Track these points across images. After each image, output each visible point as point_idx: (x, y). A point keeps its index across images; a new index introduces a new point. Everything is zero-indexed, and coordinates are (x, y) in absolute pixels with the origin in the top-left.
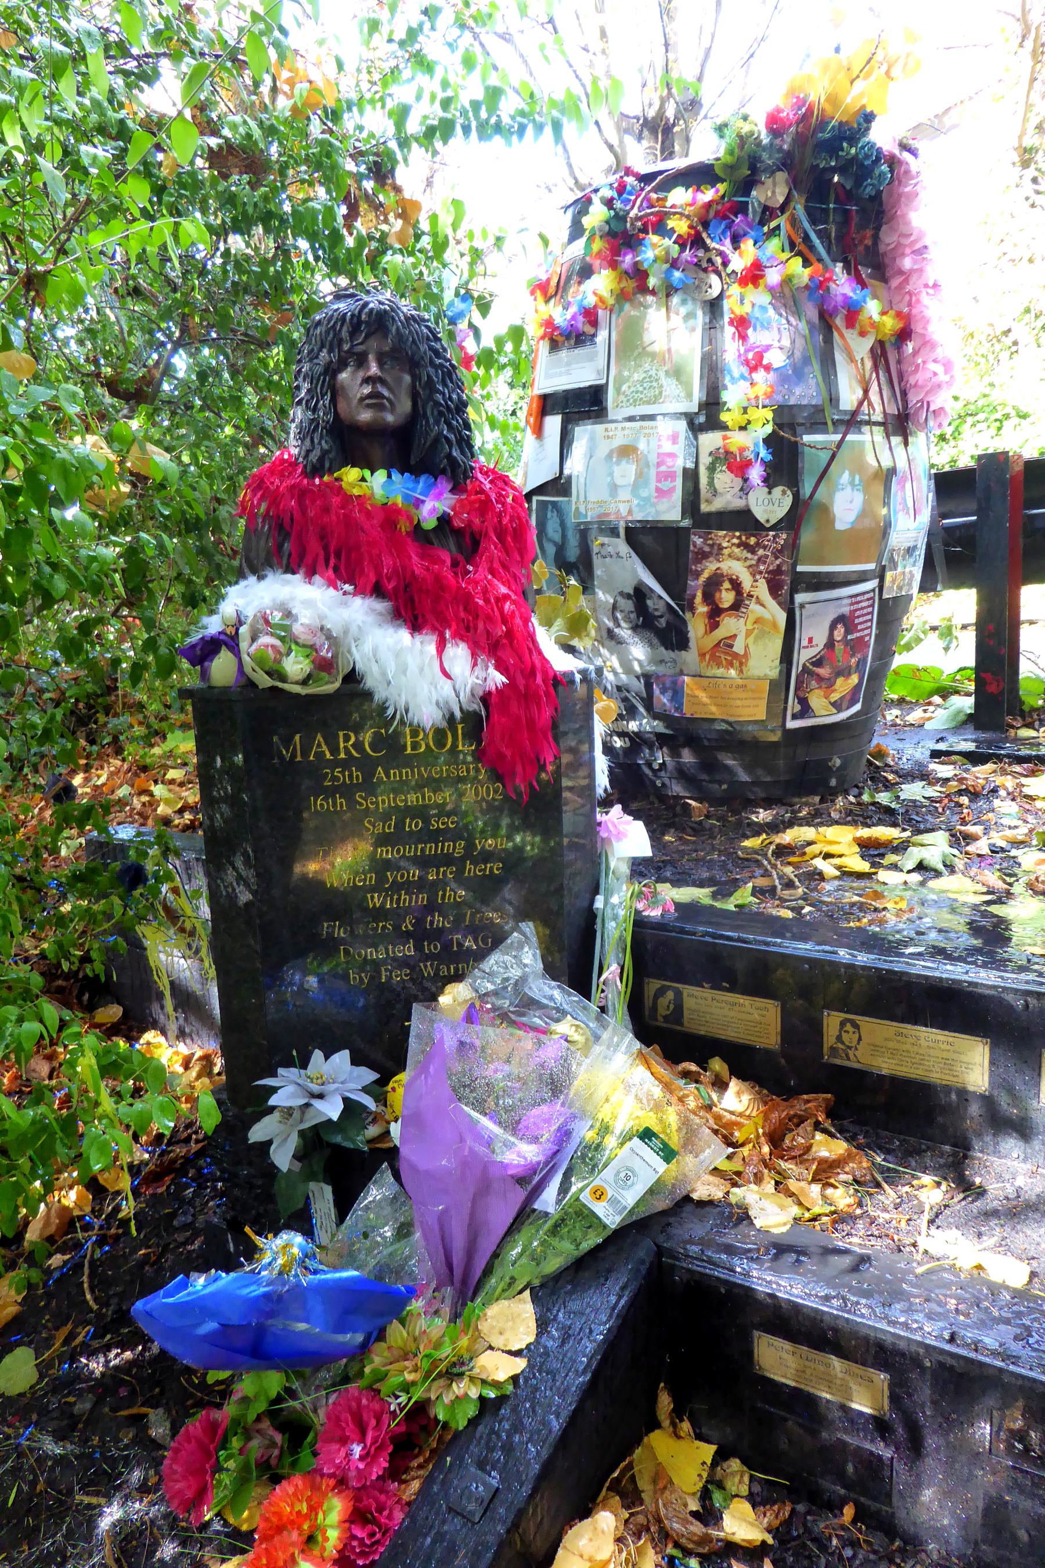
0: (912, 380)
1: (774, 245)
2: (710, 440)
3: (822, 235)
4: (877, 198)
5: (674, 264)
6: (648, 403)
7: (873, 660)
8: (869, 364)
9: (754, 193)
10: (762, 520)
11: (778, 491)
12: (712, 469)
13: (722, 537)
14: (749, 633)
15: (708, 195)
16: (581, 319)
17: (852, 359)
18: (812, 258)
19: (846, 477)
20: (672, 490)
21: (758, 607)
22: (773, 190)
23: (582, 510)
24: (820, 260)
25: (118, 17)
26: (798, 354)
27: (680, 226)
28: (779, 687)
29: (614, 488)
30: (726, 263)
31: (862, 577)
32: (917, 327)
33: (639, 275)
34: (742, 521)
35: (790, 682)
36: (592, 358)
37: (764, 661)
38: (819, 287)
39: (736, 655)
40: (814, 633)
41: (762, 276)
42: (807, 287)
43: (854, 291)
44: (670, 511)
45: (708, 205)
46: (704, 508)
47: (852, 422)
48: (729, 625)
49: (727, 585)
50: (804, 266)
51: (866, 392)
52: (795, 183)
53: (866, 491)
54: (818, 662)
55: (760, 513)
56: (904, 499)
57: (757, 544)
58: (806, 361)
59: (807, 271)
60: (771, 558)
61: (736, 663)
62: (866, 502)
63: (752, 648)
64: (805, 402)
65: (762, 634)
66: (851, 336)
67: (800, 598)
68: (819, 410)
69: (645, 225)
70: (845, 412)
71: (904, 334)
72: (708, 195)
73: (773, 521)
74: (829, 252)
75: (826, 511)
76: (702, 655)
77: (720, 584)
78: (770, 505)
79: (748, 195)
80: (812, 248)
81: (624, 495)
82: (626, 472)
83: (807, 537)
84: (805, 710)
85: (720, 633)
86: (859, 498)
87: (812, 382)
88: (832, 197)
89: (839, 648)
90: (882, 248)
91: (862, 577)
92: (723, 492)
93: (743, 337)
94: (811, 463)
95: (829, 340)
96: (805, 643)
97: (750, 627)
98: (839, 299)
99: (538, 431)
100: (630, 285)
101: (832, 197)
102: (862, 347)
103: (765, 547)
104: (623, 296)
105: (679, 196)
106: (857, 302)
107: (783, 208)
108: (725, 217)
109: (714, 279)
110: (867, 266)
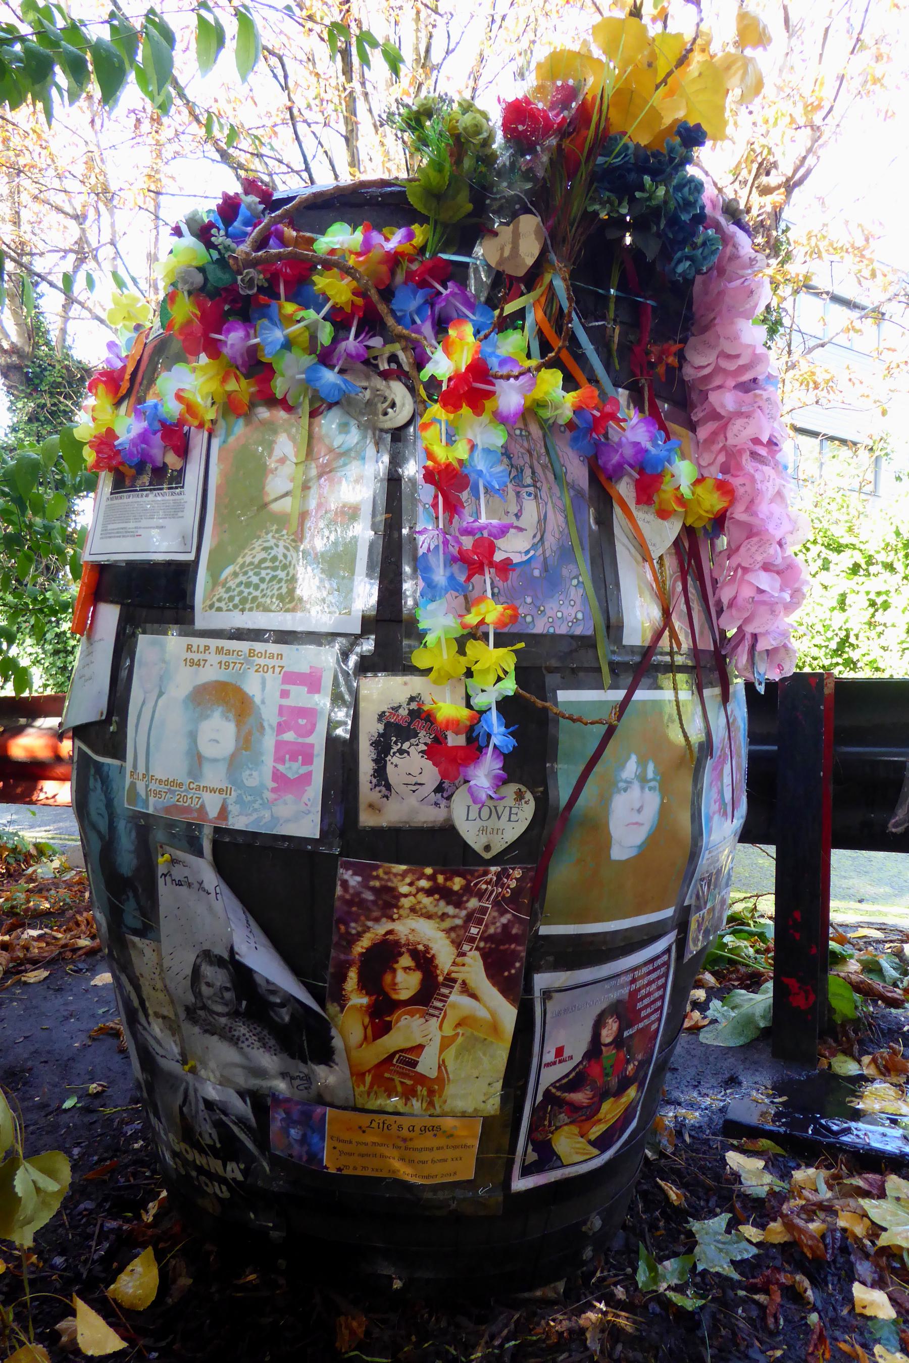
0: (726, 595)
1: (512, 344)
2: (384, 692)
3: (600, 338)
4: (682, 290)
5: (326, 358)
7: (659, 1053)
8: (671, 564)
9: (479, 250)
10: (478, 847)
12: (382, 747)
13: (401, 877)
14: (446, 1043)
15: (394, 241)
16: (157, 439)
17: (646, 557)
18: (581, 377)
19: (631, 768)
20: (306, 778)
21: (465, 1000)
22: (520, 240)
23: (141, 787)
24: (593, 380)
25: (368, 394)
26: (551, 541)
27: (336, 289)
28: (499, 1131)
29: (197, 760)
30: (421, 362)
31: (651, 934)
32: (739, 513)
33: (256, 368)
34: (438, 849)
35: (523, 1111)
36: (176, 511)
37: (475, 1088)
38: (590, 429)
39: (422, 1079)
40: (566, 1040)
41: (490, 394)
42: (571, 425)
43: (653, 439)
44: (300, 817)
45: (394, 260)
46: (366, 819)
47: (644, 667)
48: (409, 1029)
49: (406, 961)
50: (566, 388)
51: (667, 614)
52: (553, 239)
53: (664, 789)
54: (575, 1082)
55: (472, 833)
56: (721, 793)
57: (468, 890)
58: (566, 554)
59: (570, 398)
60: (491, 913)
61: (422, 1091)
62: (663, 811)
63: (451, 1065)
64: (562, 630)
65: (473, 1044)
66: (645, 518)
67: (542, 980)
68: (587, 643)
69: (273, 279)
70: (632, 649)
71: (719, 522)
72: (394, 241)
73: (494, 851)
74: (608, 366)
75: (597, 830)
76: (358, 1075)
78: (489, 815)
79: (469, 254)
80: (581, 359)
81: (214, 776)
82: (219, 733)
83: (563, 873)
84: (547, 1157)
85: (393, 1041)
86: (652, 801)
87: (575, 594)
89: (609, 1053)
90: (689, 373)
91: (651, 934)
92: (408, 792)
93: (453, 508)
94: (574, 745)
95: (605, 522)
96: (549, 1057)
97: (448, 1031)
98: (628, 452)
99: (85, 627)
100: (241, 387)
101: (615, 278)
102: (662, 535)
103: (480, 895)
104: (231, 407)
105: (340, 237)
106: (659, 461)
107: (532, 278)
108: (423, 284)
109: (398, 390)
110: (666, 400)
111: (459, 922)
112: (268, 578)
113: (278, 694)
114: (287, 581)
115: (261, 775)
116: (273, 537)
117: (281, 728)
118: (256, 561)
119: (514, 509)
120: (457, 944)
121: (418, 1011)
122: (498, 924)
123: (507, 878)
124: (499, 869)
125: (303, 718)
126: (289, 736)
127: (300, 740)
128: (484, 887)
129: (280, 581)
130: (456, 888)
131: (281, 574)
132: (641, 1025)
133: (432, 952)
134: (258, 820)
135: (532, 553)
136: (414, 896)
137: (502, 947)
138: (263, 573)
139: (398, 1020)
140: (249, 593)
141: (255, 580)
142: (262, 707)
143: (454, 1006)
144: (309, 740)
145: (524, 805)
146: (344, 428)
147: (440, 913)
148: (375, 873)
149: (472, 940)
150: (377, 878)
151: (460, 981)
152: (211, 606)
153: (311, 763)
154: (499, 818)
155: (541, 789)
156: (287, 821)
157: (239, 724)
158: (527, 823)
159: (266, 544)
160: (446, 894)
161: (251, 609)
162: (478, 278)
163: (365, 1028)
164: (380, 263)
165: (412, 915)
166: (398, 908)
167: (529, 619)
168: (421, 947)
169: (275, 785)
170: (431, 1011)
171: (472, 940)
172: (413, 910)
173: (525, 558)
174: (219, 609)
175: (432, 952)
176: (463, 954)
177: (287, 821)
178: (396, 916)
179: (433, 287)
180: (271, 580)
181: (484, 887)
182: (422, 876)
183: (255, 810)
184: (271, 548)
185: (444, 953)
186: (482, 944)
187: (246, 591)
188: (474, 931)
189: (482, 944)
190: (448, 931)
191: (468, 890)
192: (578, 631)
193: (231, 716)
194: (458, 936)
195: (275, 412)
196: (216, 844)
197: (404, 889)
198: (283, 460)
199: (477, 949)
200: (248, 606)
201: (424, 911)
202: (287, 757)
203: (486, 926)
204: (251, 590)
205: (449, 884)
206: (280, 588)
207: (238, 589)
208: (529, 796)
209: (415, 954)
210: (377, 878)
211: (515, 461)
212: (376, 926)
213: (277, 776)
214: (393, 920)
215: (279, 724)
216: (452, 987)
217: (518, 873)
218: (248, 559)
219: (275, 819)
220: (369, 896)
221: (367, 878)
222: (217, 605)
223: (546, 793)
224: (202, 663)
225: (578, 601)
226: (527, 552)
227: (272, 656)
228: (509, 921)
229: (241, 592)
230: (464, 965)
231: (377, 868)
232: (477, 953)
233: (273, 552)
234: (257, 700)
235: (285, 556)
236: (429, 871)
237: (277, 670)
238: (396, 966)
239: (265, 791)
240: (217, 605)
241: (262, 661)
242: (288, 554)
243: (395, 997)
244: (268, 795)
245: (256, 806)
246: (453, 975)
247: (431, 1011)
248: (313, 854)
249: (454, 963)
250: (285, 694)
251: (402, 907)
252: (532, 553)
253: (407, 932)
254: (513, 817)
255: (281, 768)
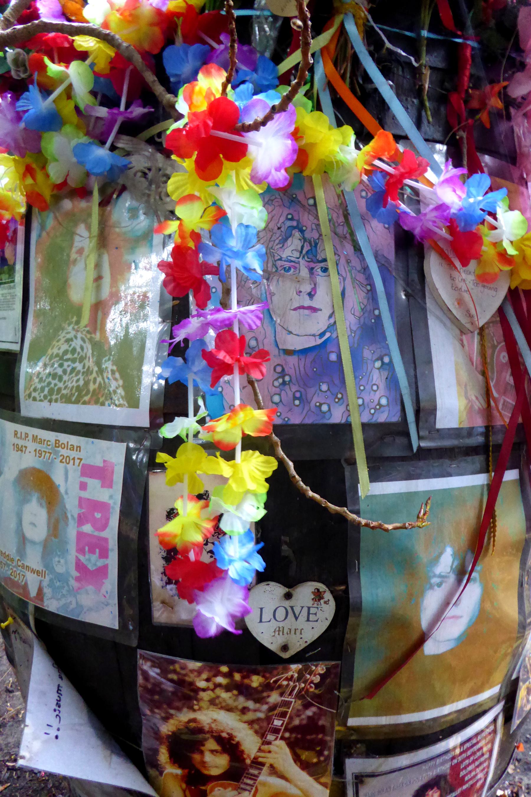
6: (67, 400)
11: (305, 592)
20: (103, 571)
49: (211, 744)
55: (266, 634)
67: (354, 765)
74: (418, 124)
77: (202, 743)
80: (380, 109)
81: (33, 559)
88: (426, 17)
101: (426, 17)
111: (261, 715)
112: (69, 370)
113: (78, 486)
114: (83, 373)
115: (66, 564)
116: (73, 328)
117: (81, 520)
118: (61, 352)
119: (307, 288)
120: (262, 734)
121: (230, 785)
122: (303, 717)
123: (310, 674)
124: (300, 666)
125: (98, 512)
126: (87, 528)
127: (96, 533)
128: (285, 683)
129: (79, 372)
130: (255, 684)
131: (79, 366)
132: (465, 787)
133: (237, 739)
134: (66, 606)
135: (328, 335)
136: (213, 690)
137: (309, 737)
138: (66, 364)
139: (212, 790)
140: (55, 385)
141: (60, 371)
142: (65, 497)
143: (264, 784)
144: (103, 534)
145: (323, 605)
146: (133, 213)
147: (240, 707)
148: (171, 667)
149: (276, 731)
150: (175, 671)
151: (267, 765)
152: (29, 395)
153: (107, 557)
154: (296, 618)
155: (343, 587)
156: (90, 609)
157: (50, 512)
158: (327, 623)
159: (69, 336)
160: (243, 690)
161: (56, 401)
162: (262, 29)
163: (184, 791)
164: (152, 24)
165: (212, 708)
166: (198, 700)
167: (325, 408)
168: (224, 735)
169: (78, 574)
170: (242, 786)
171: (276, 731)
172: (213, 702)
173: (319, 341)
174: (35, 399)
175: (237, 739)
176: (269, 743)
177: (90, 609)
178: (196, 707)
179: (204, 43)
180: (71, 372)
181: (285, 683)
182: (218, 673)
183: (64, 596)
184: (71, 340)
185: (249, 742)
186: (287, 735)
187: (53, 382)
188: (277, 723)
189: (287, 735)
190: (251, 723)
191: (268, 687)
192: (382, 418)
193: (44, 504)
194: (261, 728)
195: (76, 203)
196: (36, 620)
197: (202, 684)
198: (80, 251)
199: (282, 738)
200: (54, 397)
201: (224, 704)
202: (87, 548)
203: (291, 718)
204: (56, 381)
205: (246, 681)
206: (78, 381)
207: (47, 380)
208: (328, 596)
209: (219, 739)
210: (175, 671)
211: (307, 235)
212: (178, 714)
213: (80, 566)
214: (194, 711)
215: (79, 516)
216: (261, 769)
217: (321, 669)
218: (55, 351)
219: (79, 606)
220: (169, 687)
221: (164, 673)
222: (33, 394)
223: (346, 591)
224: (24, 449)
225: (382, 386)
226: (322, 335)
227: (72, 448)
228: (315, 713)
229: (49, 384)
230: (270, 752)
231: (173, 662)
232: (283, 744)
233: (73, 344)
234: (62, 490)
235: (82, 348)
236: (224, 669)
237: (77, 462)
238: (202, 748)
239: (71, 579)
240: (33, 394)
241: (65, 452)
242: (85, 346)
243: (206, 772)
244: (73, 583)
245: (64, 592)
246: (260, 760)
247: (242, 786)
248: (115, 645)
249: (260, 750)
250: (83, 486)
251: (202, 699)
252: (328, 335)
253: (209, 721)
254: (312, 617)
255: (81, 557)
